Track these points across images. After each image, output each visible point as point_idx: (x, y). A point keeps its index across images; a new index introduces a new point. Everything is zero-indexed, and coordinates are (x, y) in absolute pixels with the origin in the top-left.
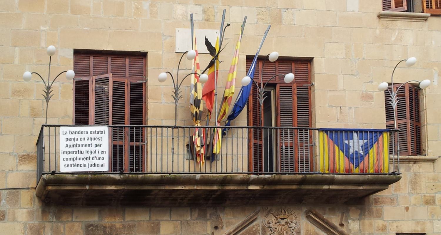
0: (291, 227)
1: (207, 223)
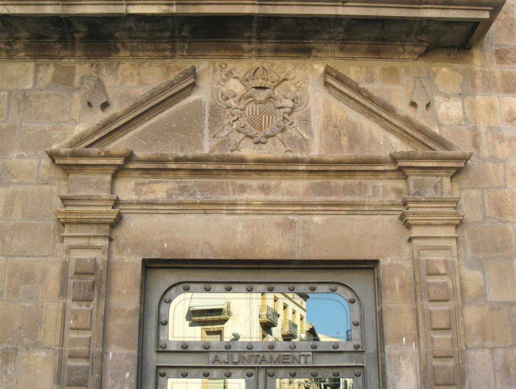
1: (72, 97)
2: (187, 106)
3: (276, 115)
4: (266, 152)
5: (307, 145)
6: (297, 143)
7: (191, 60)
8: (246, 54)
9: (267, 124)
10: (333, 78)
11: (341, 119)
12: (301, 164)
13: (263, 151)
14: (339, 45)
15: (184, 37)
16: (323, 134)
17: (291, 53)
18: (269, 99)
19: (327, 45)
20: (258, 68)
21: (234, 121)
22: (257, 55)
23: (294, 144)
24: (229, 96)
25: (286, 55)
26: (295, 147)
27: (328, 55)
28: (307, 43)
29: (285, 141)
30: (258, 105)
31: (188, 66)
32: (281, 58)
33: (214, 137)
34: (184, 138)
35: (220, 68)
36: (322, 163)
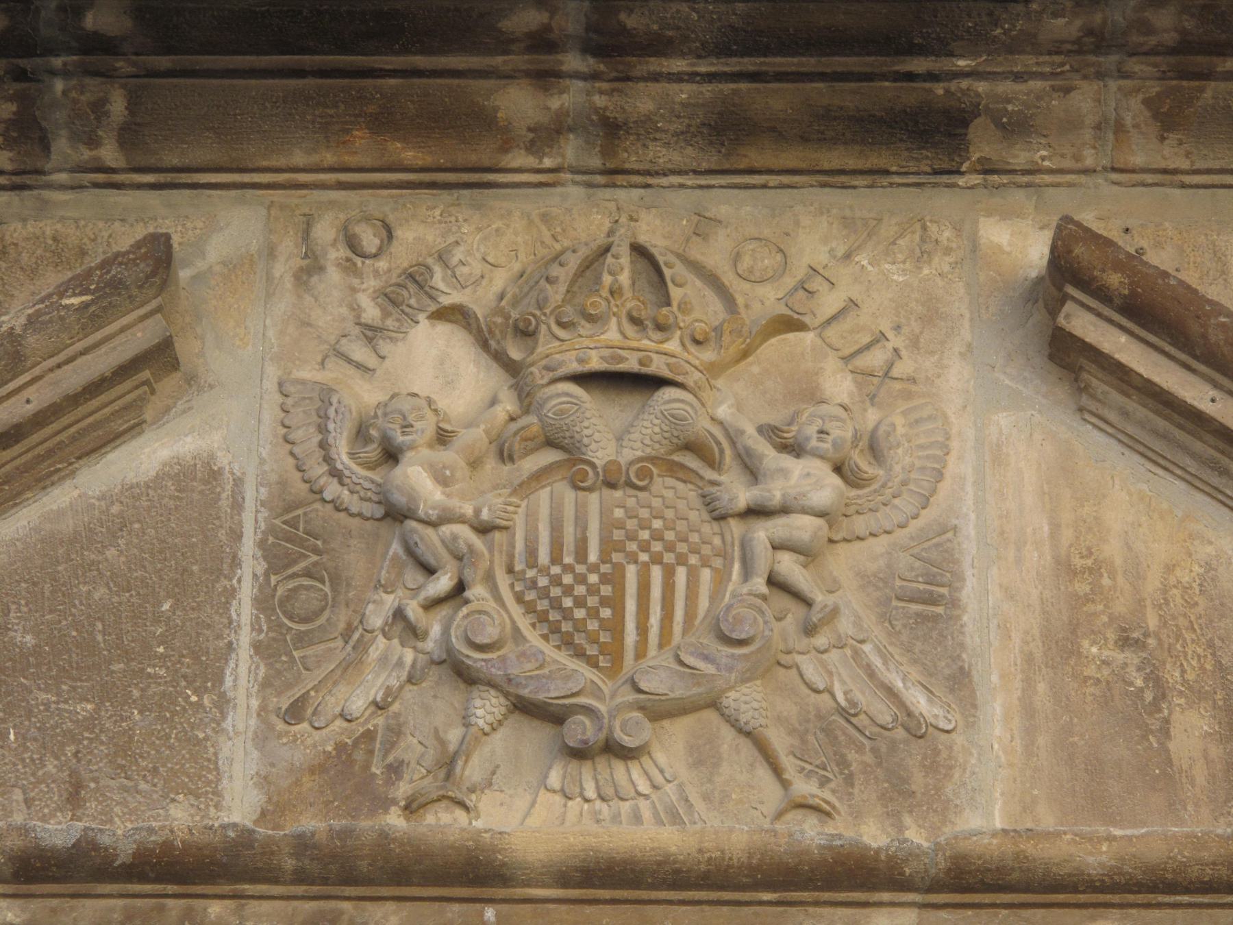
0: (756, 512)
2: (115, 509)
4: (646, 814)
6: (860, 749)
7: (153, 199)
8: (519, 159)
9: (655, 620)
10: (1107, 311)
11: (1165, 591)
12: (886, 896)
13: (626, 807)
14: (1154, 88)
15: (101, 45)
16: (1042, 687)
17: (823, 141)
19: (1067, 90)
22: (596, 162)
23: (843, 763)
25: (790, 158)
26: (849, 780)
27: (1077, 158)
28: (933, 77)
29: (779, 741)
30: (594, 498)
31: (126, 237)
33: (295, 713)
34: (90, 723)
35: (342, 252)
36: (1027, 889)
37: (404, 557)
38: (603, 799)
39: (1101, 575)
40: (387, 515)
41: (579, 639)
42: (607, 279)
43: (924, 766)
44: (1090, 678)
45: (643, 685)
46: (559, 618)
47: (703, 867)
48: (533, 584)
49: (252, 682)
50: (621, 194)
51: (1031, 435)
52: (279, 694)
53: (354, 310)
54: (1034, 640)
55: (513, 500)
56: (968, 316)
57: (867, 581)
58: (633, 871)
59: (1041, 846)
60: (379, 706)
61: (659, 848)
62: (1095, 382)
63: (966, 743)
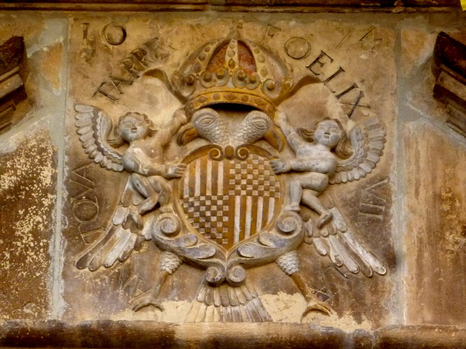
3: (279, 195)
5: (375, 292)
6: (342, 282)
18: (257, 144)
20: (226, 43)
21: (145, 213)
23: (334, 290)
24: (131, 135)
30: (221, 165)
32: (299, 9)
37: (132, 190)
38: (223, 306)
39: (455, 201)
40: (125, 170)
41: (214, 231)
42: (227, 58)
43: (371, 291)
44: (448, 250)
45: (242, 253)
46: (204, 221)
47: (269, 342)
48: (192, 205)
49: (62, 248)
50: (233, 15)
51: (424, 134)
52: (74, 254)
53: (109, 70)
54: (423, 232)
55: (183, 164)
56: (395, 75)
57: (346, 203)
58: (237, 343)
59: (424, 333)
60: (121, 261)
61: (249, 333)
62: (454, 109)
63: (391, 280)
